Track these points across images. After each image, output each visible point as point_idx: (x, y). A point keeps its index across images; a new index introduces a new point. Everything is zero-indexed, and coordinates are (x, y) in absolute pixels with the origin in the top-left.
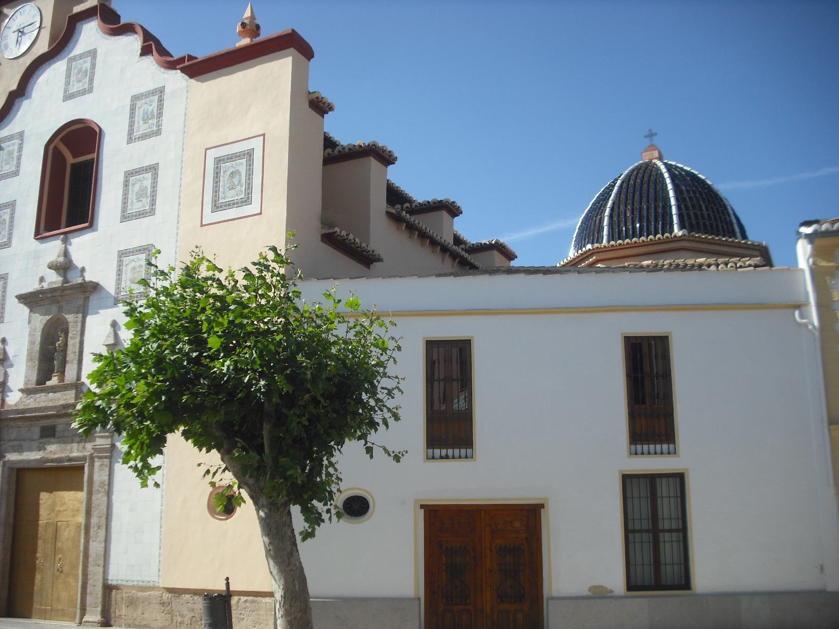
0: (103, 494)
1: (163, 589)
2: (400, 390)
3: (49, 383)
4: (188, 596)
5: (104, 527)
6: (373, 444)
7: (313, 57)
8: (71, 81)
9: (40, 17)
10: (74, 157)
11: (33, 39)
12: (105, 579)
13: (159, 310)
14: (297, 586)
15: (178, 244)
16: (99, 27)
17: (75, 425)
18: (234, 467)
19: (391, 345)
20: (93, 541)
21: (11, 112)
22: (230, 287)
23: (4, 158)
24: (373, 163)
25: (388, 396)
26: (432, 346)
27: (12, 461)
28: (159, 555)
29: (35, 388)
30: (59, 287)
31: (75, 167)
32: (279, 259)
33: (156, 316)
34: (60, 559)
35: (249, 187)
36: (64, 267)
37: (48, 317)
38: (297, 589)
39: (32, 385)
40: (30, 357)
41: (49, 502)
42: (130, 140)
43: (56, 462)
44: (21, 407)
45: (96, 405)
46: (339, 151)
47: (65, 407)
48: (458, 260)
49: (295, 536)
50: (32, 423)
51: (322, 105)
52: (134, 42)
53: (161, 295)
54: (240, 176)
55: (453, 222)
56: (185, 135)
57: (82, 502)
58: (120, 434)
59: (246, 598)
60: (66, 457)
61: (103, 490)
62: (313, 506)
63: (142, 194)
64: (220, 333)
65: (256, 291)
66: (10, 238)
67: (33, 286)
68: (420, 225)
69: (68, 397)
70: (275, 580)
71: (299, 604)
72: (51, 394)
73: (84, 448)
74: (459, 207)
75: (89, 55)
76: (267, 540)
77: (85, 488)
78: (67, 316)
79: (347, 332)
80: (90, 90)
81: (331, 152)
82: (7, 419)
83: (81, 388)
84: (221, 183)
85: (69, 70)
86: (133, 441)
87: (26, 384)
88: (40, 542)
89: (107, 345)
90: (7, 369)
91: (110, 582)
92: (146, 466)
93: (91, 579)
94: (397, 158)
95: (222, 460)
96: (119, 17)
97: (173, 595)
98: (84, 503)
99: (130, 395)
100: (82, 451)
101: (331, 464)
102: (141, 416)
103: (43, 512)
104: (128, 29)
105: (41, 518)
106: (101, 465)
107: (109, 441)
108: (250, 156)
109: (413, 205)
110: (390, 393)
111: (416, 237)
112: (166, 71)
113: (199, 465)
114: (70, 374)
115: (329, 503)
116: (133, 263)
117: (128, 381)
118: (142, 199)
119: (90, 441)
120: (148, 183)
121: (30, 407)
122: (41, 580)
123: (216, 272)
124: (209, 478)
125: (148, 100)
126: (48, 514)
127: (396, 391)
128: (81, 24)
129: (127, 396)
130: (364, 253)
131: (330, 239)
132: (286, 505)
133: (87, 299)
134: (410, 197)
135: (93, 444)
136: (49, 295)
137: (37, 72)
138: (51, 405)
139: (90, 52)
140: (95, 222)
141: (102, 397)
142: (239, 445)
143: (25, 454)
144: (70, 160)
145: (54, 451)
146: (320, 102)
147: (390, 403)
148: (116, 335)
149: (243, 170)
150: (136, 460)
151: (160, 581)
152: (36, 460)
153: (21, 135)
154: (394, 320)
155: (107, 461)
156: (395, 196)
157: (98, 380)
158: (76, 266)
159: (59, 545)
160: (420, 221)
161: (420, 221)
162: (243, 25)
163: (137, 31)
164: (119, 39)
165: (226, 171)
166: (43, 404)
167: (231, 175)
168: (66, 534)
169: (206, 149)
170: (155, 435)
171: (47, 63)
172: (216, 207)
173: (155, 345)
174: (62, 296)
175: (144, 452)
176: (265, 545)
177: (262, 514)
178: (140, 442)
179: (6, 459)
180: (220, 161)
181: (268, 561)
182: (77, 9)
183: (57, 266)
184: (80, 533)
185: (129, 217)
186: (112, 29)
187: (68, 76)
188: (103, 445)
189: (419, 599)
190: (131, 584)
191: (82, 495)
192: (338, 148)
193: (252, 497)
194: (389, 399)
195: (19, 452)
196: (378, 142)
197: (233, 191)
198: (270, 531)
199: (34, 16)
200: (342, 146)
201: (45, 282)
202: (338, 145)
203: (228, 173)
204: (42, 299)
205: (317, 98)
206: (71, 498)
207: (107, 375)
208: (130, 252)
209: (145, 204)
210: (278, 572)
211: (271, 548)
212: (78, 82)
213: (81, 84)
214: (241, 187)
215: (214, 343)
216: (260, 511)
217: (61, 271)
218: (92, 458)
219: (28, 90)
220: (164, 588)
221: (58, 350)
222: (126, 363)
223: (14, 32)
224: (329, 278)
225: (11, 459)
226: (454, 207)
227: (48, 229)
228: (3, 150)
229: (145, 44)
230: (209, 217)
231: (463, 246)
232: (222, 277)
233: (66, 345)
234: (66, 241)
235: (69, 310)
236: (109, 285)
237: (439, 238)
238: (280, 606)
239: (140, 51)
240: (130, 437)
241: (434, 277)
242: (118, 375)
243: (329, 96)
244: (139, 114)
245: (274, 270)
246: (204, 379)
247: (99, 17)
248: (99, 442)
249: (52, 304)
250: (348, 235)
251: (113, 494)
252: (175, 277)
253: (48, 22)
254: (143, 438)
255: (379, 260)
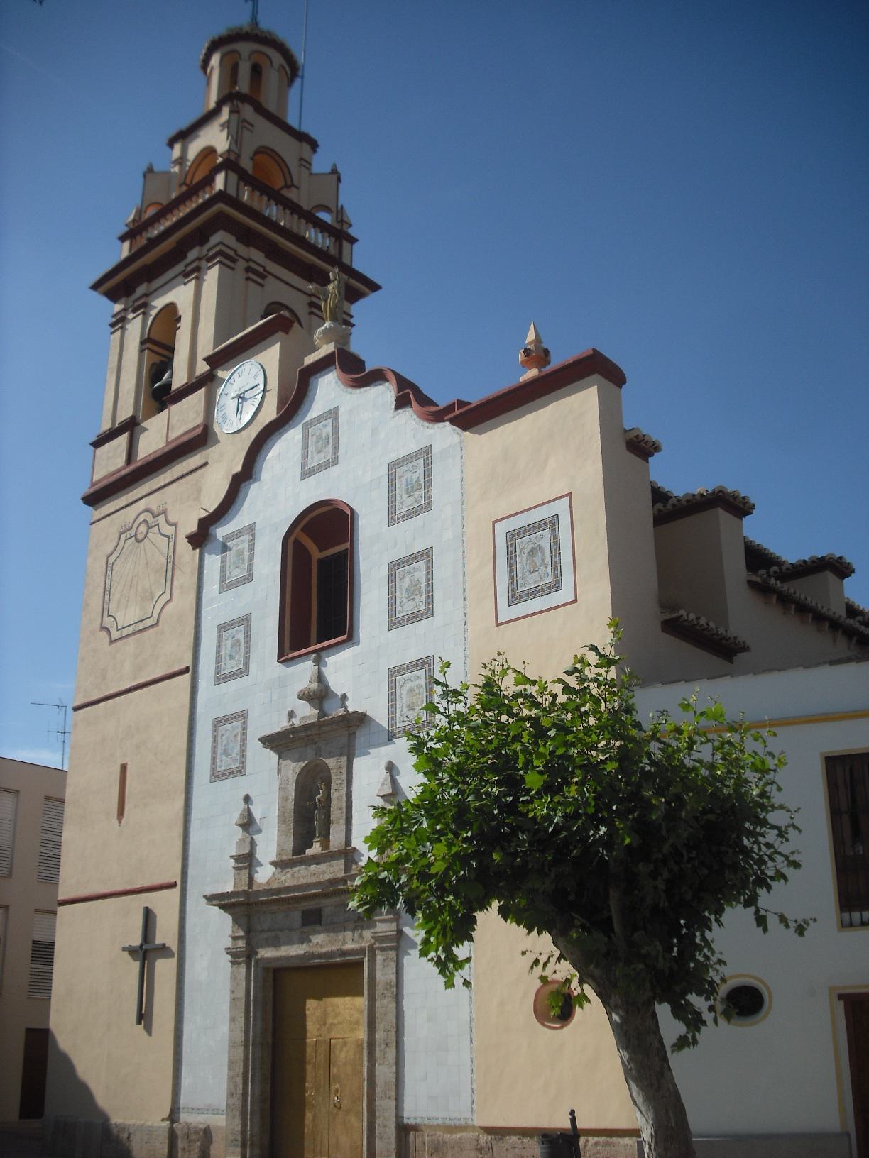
0: (390, 998)
1: (479, 1129)
2: (795, 827)
3: (309, 852)
4: (514, 1138)
5: (395, 1044)
6: (766, 911)
7: (625, 383)
8: (309, 452)
9: (263, 376)
10: (321, 550)
11: (257, 404)
12: (399, 1117)
13: (454, 742)
14: (672, 1120)
15: (468, 652)
16: (339, 379)
17: (352, 904)
18: (572, 953)
19: (771, 763)
20: (379, 1065)
21: (237, 500)
22: (546, 704)
23: (232, 561)
24: (723, 516)
25: (780, 839)
26: (833, 763)
27: (267, 959)
28: (472, 1081)
29: (292, 860)
30: (314, 723)
31: (321, 562)
32: (606, 662)
33: (451, 752)
34: (337, 1091)
35: (557, 567)
36: (319, 695)
37: (302, 764)
38: (673, 1125)
39: (288, 856)
40: (283, 818)
41: (319, 1013)
42: (392, 521)
43: (325, 958)
44: (275, 886)
45: (380, 877)
46: (674, 505)
47: (333, 882)
48: (855, 638)
49: (665, 1047)
50: (290, 906)
51: (644, 445)
52: (385, 393)
53: (456, 723)
54: (543, 553)
55: (842, 586)
56: (464, 506)
57: (362, 1012)
58: (413, 915)
59: (596, 1139)
60: (338, 950)
61: (389, 994)
62: (688, 1002)
63: (414, 591)
64: (541, 768)
65: (578, 708)
66: (247, 664)
67: (279, 724)
68: (798, 594)
69: (335, 869)
70: (641, 1112)
71: (677, 1146)
72: (313, 867)
73: (361, 936)
74: (849, 563)
75: (329, 416)
76: (625, 1054)
77: (366, 992)
78: (327, 761)
79: (713, 754)
80: (335, 461)
81: (662, 508)
82: (256, 903)
83: (352, 856)
84: (519, 566)
85: (305, 438)
86: (431, 924)
87: (279, 854)
88: (309, 1068)
89: (382, 796)
90: (253, 837)
91: (405, 1121)
92: (451, 958)
93: (379, 1117)
94: (754, 505)
95: (555, 944)
96: (363, 363)
97: (493, 1137)
98: (366, 1013)
99: (424, 862)
100: (358, 942)
101: (707, 944)
102: (441, 890)
103: (311, 1027)
104: (376, 377)
105: (308, 1035)
106: (385, 960)
107: (393, 926)
108: (554, 525)
109: (784, 568)
110: (782, 834)
111: (793, 612)
112: (431, 425)
113: (524, 953)
114: (336, 839)
115: (712, 997)
116: (410, 683)
117: (419, 841)
118: (415, 597)
119: (368, 928)
120: (420, 575)
121: (287, 884)
122: (314, 1120)
123: (528, 686)
124: (538, 970)
125: (410, 465)
126: (318, 1030)
127: (791, 830)
128: (316, 378)
129: (420, 864)
130: (724, 642)
131: (674, 627)
132: (649, 1004)
133: (352, 736)
134: (778, 558)
135: (372, 931)
136: (302, 734)
137: (265, 446)
138: (314, 881)
139: (329, 412)
140: (355, 634)
141: (388, 867)
142: (577, 923)
143: (283, 948)
144: (316, 555)
145: (321, 943)
146: (642, 441)
147: (785, 848)
148: (394, 782)
149: (546, 545)
150: (437, 951)
151: (475, 1117)
152: (298, 957)
153: (251, 529)
154: (774, 729)
155: (392, 954)
156: (757, 558)
157: (379, 844)
158: (333, 692)
159: (334, 1070)
160: (796, 588)
161: (796, 588)
162: (527, 352)
163: (388, 378)
164: (366, 391)
165: (522, 549)
166: (303, 881)
167: (531, 553)
168: (343, 1055)
169: (494, 523)
170: (460, 915)
171: (277, 433)
172: (515, 598)
173: (454, 792)
174: (319, 734)
175: (448, 939)
176: (623, 1062)
177: (615, 1017)
178: (441, 925)
179: (259, 957)
180: (514, 535)
181: (628, 1085)
182: (309, 360)
183: (310, 695)
184: (362, 1055)
185: (399, 622)
186: (356, 380)
187: (305, 447)
188: (386, 932)
189: (848, 1135)
190: (434, 1122)
191: (362, 1002)
192: (671, 502)
193: (599, 995)
194: (782, 843)
195: (275, 946)
196: (726, 487)
197: (535, 574)
198: (629, 1041)
199: (255, 377)
200: (676, 497)
201: (296, 717)
202: (671, 497)
203: (527, 551)
204: (293, 741)
205: (637, 436)
206: (347, 1006)
207: (391, 837)
208: (404, 669)
209: (418, 604)
210: (644, 1101)
211: (632, 1066)
212: (318, 453)
213: (322, 455)
214: (546, 567)
215: (534, 780)
216: (613, 1014)
217: (316, 701)
218: (372, 950)
219: (256, 470)
220: (480, 1127)
221: (318, 806)
222: (415, 818)
223: (233, 398)
224: (679, 681)
225: (266, 956)
226: (842, 564)
227: (295, 647)
228: (230, 550)
229: (400, 394)
230: (506, 613)
231: (860, 618)
232: (533, 690)
233: (328, 799)
234: (318, 662)
235: (330, 753)
236: (380, 715)
237: (824, 610)
238: (650, 1149)
239: (394, 403)
240: (427, 918)
241: (828, 666)
242: (406, 835)
243: (651, 431)
244: (400, 485)
245: (599, 678)
246: (523, 833)
247: (337, 367)
248: (381, 927)
249: (306, 746)
250: (698, 619)
251: (403, 998)
252: (471, 697)
253: (274, 383)
254: (444, 920)
255: (745, 649)
